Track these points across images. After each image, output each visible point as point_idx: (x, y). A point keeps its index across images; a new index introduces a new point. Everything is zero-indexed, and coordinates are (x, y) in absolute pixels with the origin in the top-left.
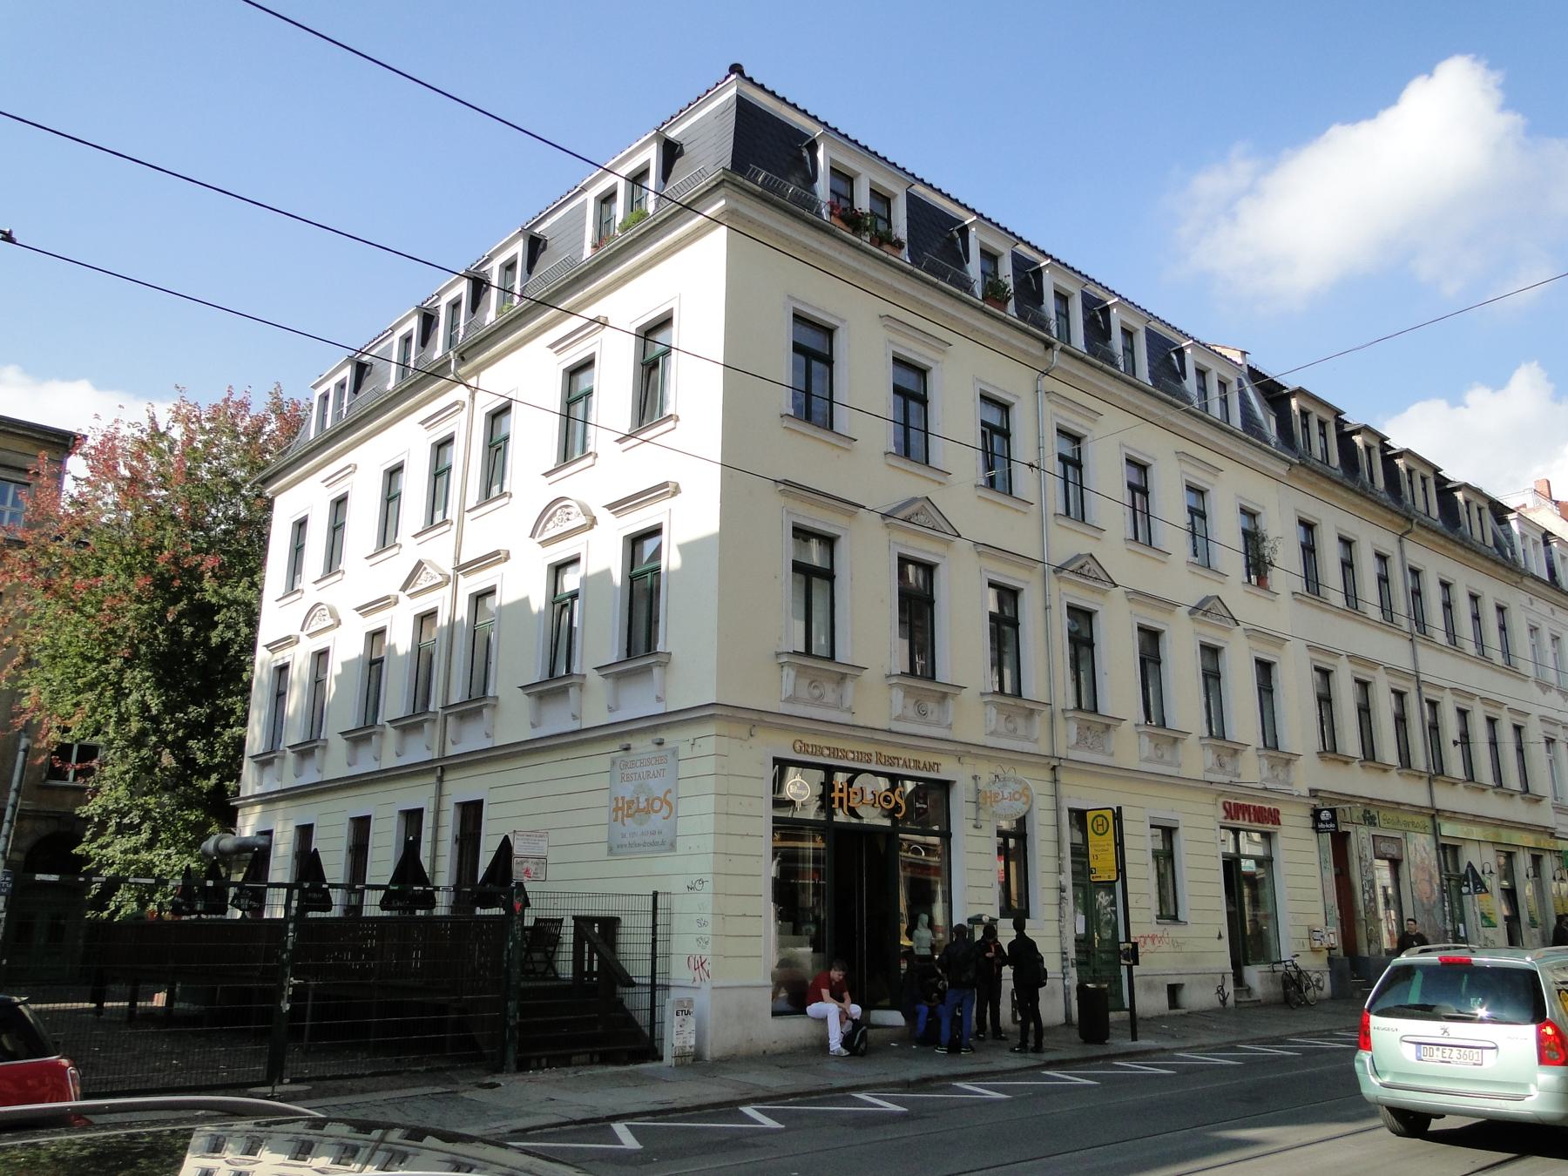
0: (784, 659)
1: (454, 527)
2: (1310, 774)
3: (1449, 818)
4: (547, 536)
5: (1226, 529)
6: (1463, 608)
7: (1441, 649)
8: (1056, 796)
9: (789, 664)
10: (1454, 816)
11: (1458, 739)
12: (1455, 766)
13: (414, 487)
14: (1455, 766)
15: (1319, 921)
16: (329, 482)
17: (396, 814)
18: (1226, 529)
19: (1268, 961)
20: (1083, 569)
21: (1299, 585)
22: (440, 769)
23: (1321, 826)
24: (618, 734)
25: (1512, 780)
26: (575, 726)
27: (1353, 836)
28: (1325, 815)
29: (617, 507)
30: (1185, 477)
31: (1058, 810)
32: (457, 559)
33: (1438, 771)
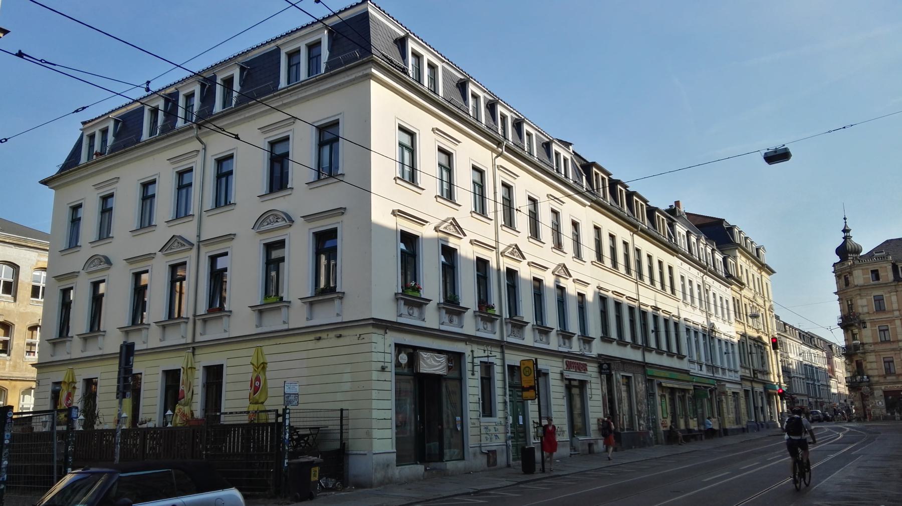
1: (196, 219)
2: (598, 348)
3: (650, 367)
4: (262, 229)
5: (464, 179)
8: (503, 359)
9: (402, 299)
10: (652, 366)
13: (165, 194)
16: (97, 186)
17: (161, 373)
19: (523, 449)
21: (594, 258)
22: (193, 348)
24: (317, 332)
26: (285, 327)
28: (605, 366)
29: (308, 218)
30: (398, 122)
31: (503, 366)
32: (199, 236)
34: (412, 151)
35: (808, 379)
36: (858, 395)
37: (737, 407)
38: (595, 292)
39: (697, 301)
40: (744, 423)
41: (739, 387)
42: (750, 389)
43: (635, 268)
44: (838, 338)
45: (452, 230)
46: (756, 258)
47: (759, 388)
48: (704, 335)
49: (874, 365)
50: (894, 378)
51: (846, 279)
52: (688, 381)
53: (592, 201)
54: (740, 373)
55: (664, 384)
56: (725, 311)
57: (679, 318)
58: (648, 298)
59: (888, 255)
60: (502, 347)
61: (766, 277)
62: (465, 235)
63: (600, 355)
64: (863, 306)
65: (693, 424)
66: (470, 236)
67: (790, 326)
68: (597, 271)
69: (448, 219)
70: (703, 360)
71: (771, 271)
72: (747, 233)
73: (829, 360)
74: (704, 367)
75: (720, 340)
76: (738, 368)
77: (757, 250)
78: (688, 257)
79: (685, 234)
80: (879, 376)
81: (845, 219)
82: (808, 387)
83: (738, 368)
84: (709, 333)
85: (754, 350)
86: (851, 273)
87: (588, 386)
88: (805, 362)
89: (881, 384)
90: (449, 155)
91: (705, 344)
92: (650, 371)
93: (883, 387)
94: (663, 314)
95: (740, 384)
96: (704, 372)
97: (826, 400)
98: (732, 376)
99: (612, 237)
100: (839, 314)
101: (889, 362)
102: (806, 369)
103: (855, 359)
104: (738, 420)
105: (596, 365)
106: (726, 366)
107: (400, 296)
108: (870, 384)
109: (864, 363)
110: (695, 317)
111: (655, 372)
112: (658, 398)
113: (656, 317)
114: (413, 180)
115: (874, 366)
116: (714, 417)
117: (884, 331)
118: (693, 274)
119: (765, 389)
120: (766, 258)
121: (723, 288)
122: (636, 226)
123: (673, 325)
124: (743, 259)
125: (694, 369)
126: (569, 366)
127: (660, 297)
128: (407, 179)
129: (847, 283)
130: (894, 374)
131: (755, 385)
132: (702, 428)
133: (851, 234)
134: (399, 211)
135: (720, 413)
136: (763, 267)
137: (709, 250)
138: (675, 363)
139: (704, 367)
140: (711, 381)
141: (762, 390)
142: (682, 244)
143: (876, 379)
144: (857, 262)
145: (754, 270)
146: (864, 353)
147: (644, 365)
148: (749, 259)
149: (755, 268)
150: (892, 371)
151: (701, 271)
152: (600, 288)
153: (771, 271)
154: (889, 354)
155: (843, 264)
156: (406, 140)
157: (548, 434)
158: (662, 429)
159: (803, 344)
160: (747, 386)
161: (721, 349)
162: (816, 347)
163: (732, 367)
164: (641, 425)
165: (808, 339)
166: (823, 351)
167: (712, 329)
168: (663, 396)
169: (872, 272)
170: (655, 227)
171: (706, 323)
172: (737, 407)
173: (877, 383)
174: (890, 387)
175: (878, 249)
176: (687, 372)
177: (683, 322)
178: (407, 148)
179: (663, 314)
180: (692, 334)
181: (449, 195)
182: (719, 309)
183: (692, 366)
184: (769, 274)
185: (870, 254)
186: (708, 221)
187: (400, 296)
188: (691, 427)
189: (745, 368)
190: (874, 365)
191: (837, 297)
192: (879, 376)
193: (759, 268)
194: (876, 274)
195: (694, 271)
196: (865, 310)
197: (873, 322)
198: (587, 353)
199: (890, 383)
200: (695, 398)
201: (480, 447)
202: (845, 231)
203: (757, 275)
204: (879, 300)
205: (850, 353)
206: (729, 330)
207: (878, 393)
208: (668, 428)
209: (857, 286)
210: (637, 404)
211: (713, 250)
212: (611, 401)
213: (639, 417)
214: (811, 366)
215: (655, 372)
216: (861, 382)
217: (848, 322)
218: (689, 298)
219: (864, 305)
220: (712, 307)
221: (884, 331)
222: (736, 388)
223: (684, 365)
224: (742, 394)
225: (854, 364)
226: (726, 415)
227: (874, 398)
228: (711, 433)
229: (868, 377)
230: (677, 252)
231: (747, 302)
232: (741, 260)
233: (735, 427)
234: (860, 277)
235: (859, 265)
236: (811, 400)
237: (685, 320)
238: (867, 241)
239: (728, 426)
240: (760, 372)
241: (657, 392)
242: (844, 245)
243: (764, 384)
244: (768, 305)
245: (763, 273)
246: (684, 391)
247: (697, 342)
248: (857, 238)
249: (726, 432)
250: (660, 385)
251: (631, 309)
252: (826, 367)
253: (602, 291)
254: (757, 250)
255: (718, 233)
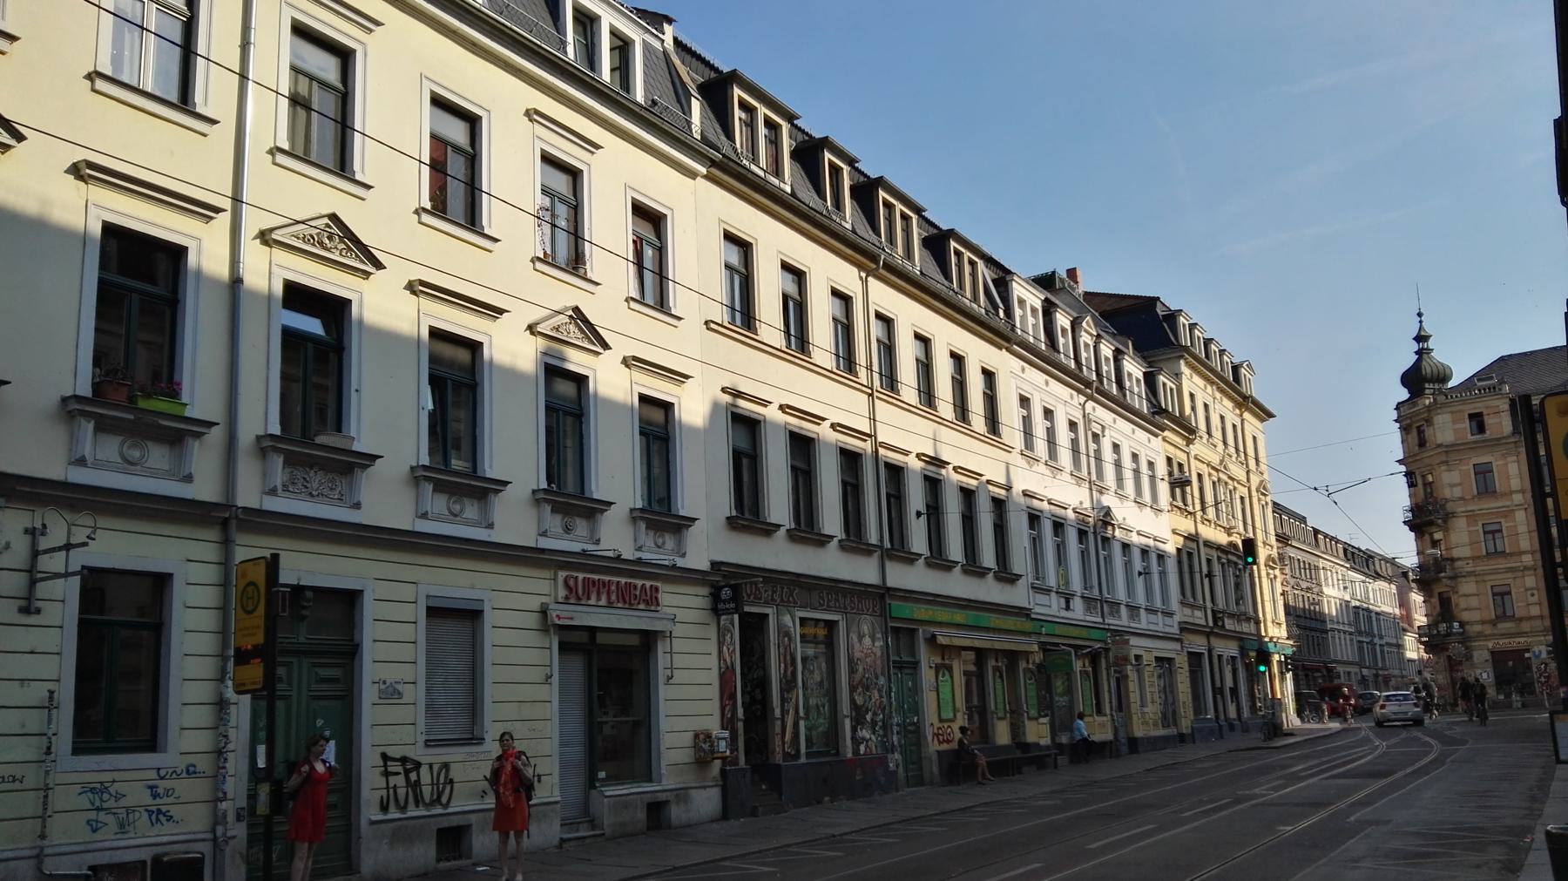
0: (75, 406)
2: (707, 544)
3: (905, 599)
5: (609, 229)
6: (1127, 462)
7: (907, 408)
10: (909, 596)
11: (923, 509)
12: (918, 540)
14: (918, 540)
15: (713, 725)
18: (609, 229)
20: (343, 240)
23: (721, 606)
25: (988, 558)
27: (771, 619)
28: (726, 593)
30: (631, 193)
33: (898, 551)
34: (576, 209)
35: (1360, 633)
36: (1443, 660)
37: (1169, 690)
38: (716, 406)
39: (1065, 456)
40: (1186, 724)
41: (1177, 646)
42: (1203, 650)
43: (865, 357)
44: (1404, 549)
45: (573, 334)
46: (1232, 383)
47: (1229, 649)
48: (1082, 534)
49: (1474, 602)
50: (1511, 625)
51: (1420, 432)
52: (1029, 634)
53: (713, 163)
54: (1177, 618)
55: (941, 640)
56: (1145, 481)
57: (1009, 488)
58: (906, 434)
59: (1502, 382)
60: (225, 524)
61: (1252, 424)
62: (606, 346)
63: (715, 565)
64: (1452, 486)
65: (1038, 732)
66: (621, 348)
67: (1326, 536)
68: (924, 426)
69: (567, 309)
70: (1076, 584)
71: (1264, 414)
72: (1207, 329)
73: (1403, 603)
74: (1077, 604)
75: (1126, 547)
76: (1174, 604)
77: (1236, 369)
78: (1046, 358)
79: (1038, 305)
80: (1483, 622)
81: (1420, 315)
82: (1361, 649)
83: (1174, 604)
84: (1097, 531)
85: (1217, 568)
86: (1429, 422)
87: (661, 647)
88: (1354, 603)
89: (1486, 637)
90: (574, 174)
91: (1084, 555)
92: (901, 609)
93: (1490, 645)
94: (955, 477)
95: (1177, 640)
96: (1078, 611)
97: (1396, 672)
98: (1155, 625)
99: (958, 360)
100: (1407, 502)
101: (1502, 594)
102: (1356, 614)
103: (1438, 589)
104: (1169, 716)
105: (705, 591)
106: (1141, 599)
107: (542, 496)
108: (1465, 639)
109: (1454, 599)
110: (1066, 494)
111: (922, 612)
112: (927, 675)
113: (933, 485)
114: (662, 304)
115: (1472, 603)
116: (1099, 711)
117: (1493, 532)
118: (1064, 400)
119: (1243, 651)
120: (1255, 386)
121: (1142, 435)
122: (874, 258)
123: (986, 511)
124: (1197, 379)
125: (1051, 607)
126: (575, 595)
127: (946, 434)
128: (650, 301)
129: (1422, 443)
130: (1512, 618)
131: (1215, 642)
132: (1064, 739)
133: (1431, 344)
134: (423, 283)
135: (1122, 704)
136: (1245, 402)
137: (1107, 350)
138: (989, 591)
139: (1077, 604)
140: (1096, 634)
141: (1235, 652)
142: (1029, 324)
143: (1477, 628)
144: (1441, 398)
145: (1224, 407)
146: (1454, 578)
147: (882, 594)
148: (1212, 383)
149: (1229, 404)
150: (1509, 613)
151: (1079, 391)
152: (738, 394)
153: (1264, 414)
154: (1500, 579)
155: (1415, 404)
156: (561, 183)
157: (512, 781)
158: (933, 747)
159: (1352, 568)
160: (1198, 644)
161: (1128, 565)
162: (1377, 576)
163: (1158, 604)
164: (861, 741)
165: (1363, 561)
166: (1390, 582)
167: (1106, 518)
168: (942, 669)
169: (1471, 416)
170: (947, 274)
171: (1087, 504)
172: (1169, 690)
173: (1480, 635)
174: (1504, 644)
175: (1481, 375)
176: (1024, 613)
177: (1022, 500)
178: (457, 149)
179: (955, 477)
180: (1047, 528)
181: (572, 258)
182: (1128, 475)
183: (1041, 598)
184: (1262, 420)
185: (1468, 384)
186: (1124, 304)
187: (542, 496)
188: (1031, 737)
189: (1192, 607)
190: (1474, 602)
191: (1403, 468)
192: (1483, 622)
193: (1238, 405)
194: (1478, 421)
195: (1064, 392)
196: (1457, 492)
197: (1471, 517)
198: (680, 563)
199: (1504, 635)
200: (1043, 674)
201: (39, 857)
202: (1421, 338)
203: (1232, 417)
204: (1483, 472)
205: (1430, 576)
206: (1151, 524)
207: (1481, 655)
208: (955, 745)
209: (1439, 446)
210: (853, 689)
211: (1118, 354)
212: (757, 685)
213: (858, 722)
214: (1367, 610)
215: (922, 612)
216: (1449, 634)
217: (1422, 520)
218: (1045, 449)
219: (1453, 482)
220: (1109, 470)
221: (1493, 533)
222: (1167, 649)
223: (1017, 595)
224: (1182, 661)
225: (1435, 600)
226: (1135, 707)
227: (1473, 666)
228: (1086, 751)
229: (1462, 625)
230: (1008, 340)
231: (1205, 470)
232: (1192, 383)
233: (1161, 732)
234: (1447, 428)
235: (1444, 405)
236: (1365, 672)
237: (1026, 494)
238: (1462, 361)
239: (1139, 732)
240: (1232, 616)
241: (926, 658)
242: (1416, 366)
243: (1241, 639)
244: (1255, 480)
245: (1247, 415)
246: (1012, 656)
247: (1060, 549)
248: (1441, 353)
249: (1134, 745)
250: (932, 640)
251: (850, 459)
252: (1397, 611)
253: (742, 403)
254: (1236, 369)
255: (1144, 326)
